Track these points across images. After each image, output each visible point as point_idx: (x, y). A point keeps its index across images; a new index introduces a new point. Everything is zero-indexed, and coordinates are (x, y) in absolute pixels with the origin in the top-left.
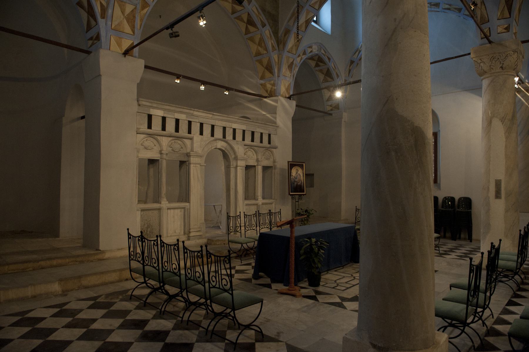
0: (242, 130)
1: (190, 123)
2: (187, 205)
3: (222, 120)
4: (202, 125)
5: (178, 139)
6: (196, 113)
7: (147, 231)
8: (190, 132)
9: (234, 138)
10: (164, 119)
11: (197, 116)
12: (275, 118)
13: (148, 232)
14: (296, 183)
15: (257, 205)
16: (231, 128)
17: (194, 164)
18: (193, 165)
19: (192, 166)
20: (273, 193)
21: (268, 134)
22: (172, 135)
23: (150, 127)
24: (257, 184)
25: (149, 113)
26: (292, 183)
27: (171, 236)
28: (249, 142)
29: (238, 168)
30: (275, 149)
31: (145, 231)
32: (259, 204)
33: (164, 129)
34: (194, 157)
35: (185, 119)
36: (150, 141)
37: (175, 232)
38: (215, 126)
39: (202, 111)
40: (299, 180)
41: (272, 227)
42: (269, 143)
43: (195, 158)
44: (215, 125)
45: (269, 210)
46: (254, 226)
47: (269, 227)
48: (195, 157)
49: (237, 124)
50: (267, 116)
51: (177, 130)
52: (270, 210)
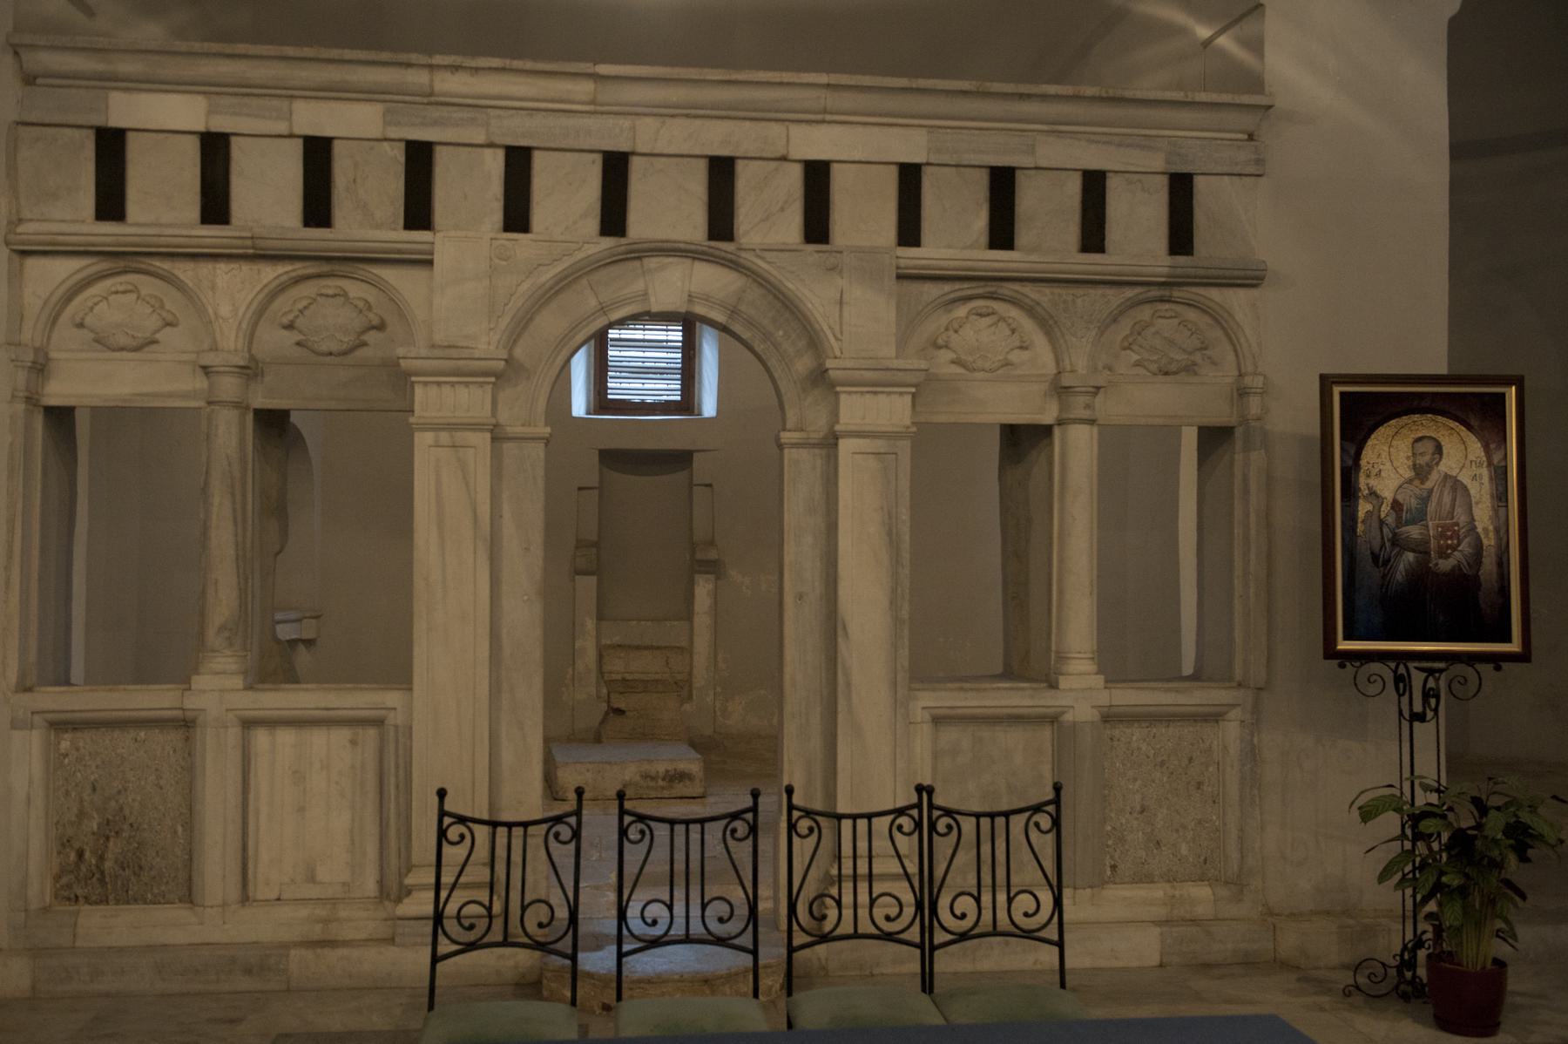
0: (894, 171)
1: (419, 158)
2: (390, 704)
3: (690, 111)
4: (518, 162)
5: (337, 267)
6: (451, 84)
7: (101, 858)
8: (418, 213)
9: (817, 228)
10: (215, 149)
11: (476, 106)
12: (1256, 45)
13: (108, 865)
14: (1410, 556)
15: (1053, 720)
16: (784, 159)
17: (436, 427)
18: (429, 437)
19: (423, 440)
20: (1238, 635)
21: (1165, 180)
22: (261, 243)
23: (111, 204)
24: (1061, 561)
25: (99, 121)
26: (1363, 551)
27: (279, 899)
28: (392, 235)
29: (845, 446)
30: (1241, 292)
31: (87, 855)
32: (1068, 717)
33: (215, 207)
34: (439, 384)
35: (379, 135)
36: (1176, 321)
37: (311, 878)
38: (636, 164)
39: (496, 62)
40: (1442, 535)
41: (940, 937)
42: (1181, 238)
43: (446, 390)
44: (634, 153)
45: (920, 789)
46: (723, 909)
47: (914, 934)
48: (453, 384)
49: (837, 130)
50: (1222, 53)
51: (317, 209)
52: (930, 791)
